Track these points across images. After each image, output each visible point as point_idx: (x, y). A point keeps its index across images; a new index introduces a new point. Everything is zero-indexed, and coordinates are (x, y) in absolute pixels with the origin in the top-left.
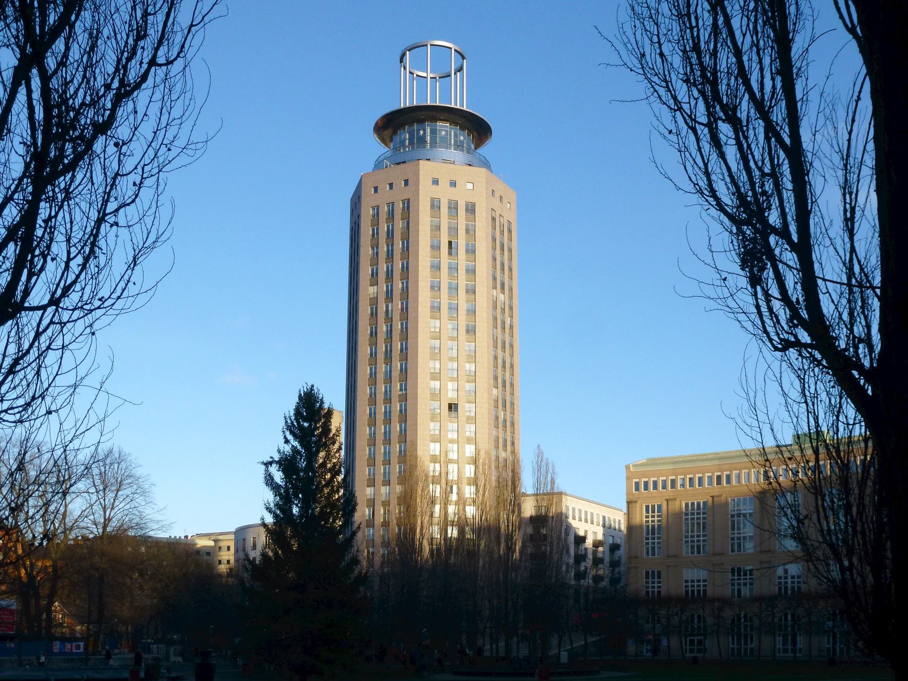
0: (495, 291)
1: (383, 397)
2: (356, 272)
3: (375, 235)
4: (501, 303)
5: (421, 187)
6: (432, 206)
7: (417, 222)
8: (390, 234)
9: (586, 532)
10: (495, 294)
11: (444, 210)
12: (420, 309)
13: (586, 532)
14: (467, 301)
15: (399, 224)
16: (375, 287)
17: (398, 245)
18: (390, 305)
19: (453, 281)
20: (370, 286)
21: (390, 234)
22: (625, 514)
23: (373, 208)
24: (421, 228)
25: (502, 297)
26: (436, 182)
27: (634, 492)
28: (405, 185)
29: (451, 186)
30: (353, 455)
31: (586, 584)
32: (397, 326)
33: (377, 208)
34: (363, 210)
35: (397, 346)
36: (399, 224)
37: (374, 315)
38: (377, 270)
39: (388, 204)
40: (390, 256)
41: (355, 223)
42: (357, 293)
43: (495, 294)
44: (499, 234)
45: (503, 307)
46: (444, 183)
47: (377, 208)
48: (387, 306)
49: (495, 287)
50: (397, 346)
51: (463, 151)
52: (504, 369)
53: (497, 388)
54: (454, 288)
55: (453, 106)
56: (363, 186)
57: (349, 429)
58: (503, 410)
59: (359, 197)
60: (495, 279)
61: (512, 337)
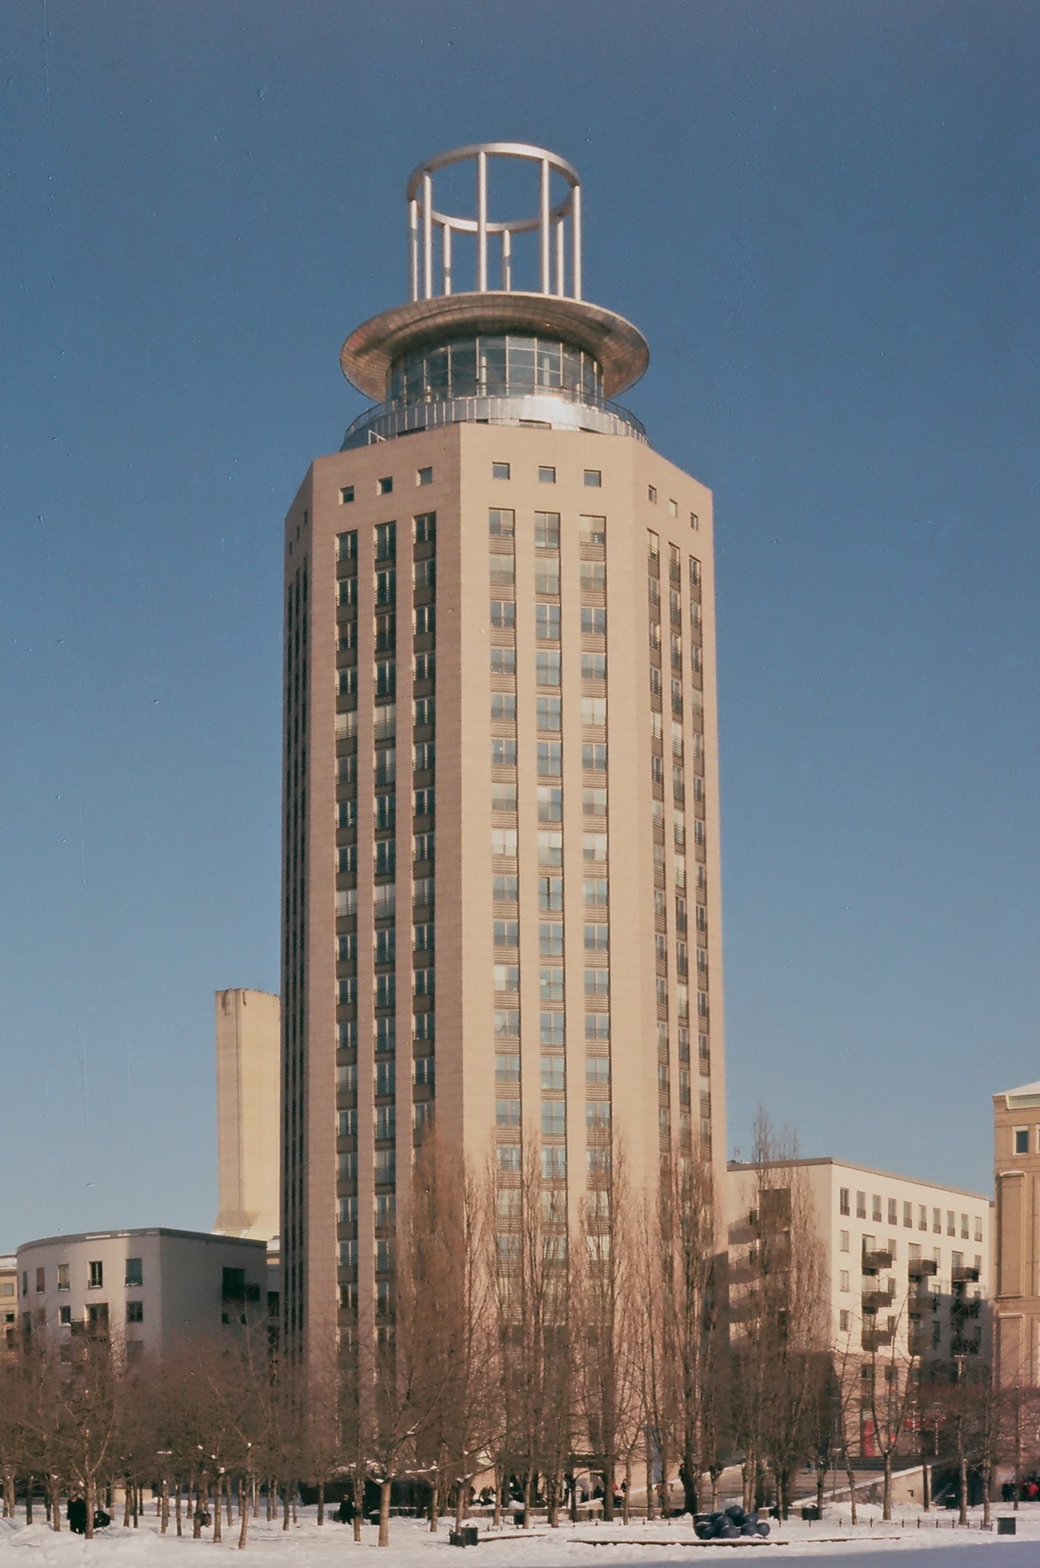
0: (658, 716)
1: (373, 1046)
2: (300, 769)
3: (349, 603)
4: (675, 743)
5: (464, 486)
6: (495, 528)
7: (456, 565)
8: (387, 598)
9: (892, 1243)
10: (658, 725)
11: (526, 537)
12: (465, 761)
13: (892, 1243)
14: (591, 1055)
15: (408, 573)
16: (350, 715)
17: (408, 619)
18: (388, 754)
19: (553, 968)
20: (339, 712)
21: (387, 598)
22: (991, 1205)
23: (342, 537)
24: (465, 578)
25: (674, 731)
26: (503, 471)
27: (1015, 1153)
28: (423, 483)
29: (541, 479)
30: (302, 1000)
31: (889, 1355)
32: (407, 799)
33: (350, 539)
34: (316, 539)
35: (407, 978)
36: (408, 573)
37: (348, 782)
38: (354, 676)
39: (380, 527)
40: (387, 644)
41: (297, 573)
42: (303, 860)
43: (658, 725)
44: (668, 587)
45: (679, 752)
46: (525, 473)
47: (350, 539)
48: (381, 759)
49: (658, 708)
50: (408, 619)
51: (574, 399)
52: (678, 673)
53: (661, 712)
54: (556, 939)
55: (546, 294)
56: (317, 485)
57: (291, 1027)
58: (683, 1155)
59: (307, 515)
60: (658, 778)
61: (704, 819)
